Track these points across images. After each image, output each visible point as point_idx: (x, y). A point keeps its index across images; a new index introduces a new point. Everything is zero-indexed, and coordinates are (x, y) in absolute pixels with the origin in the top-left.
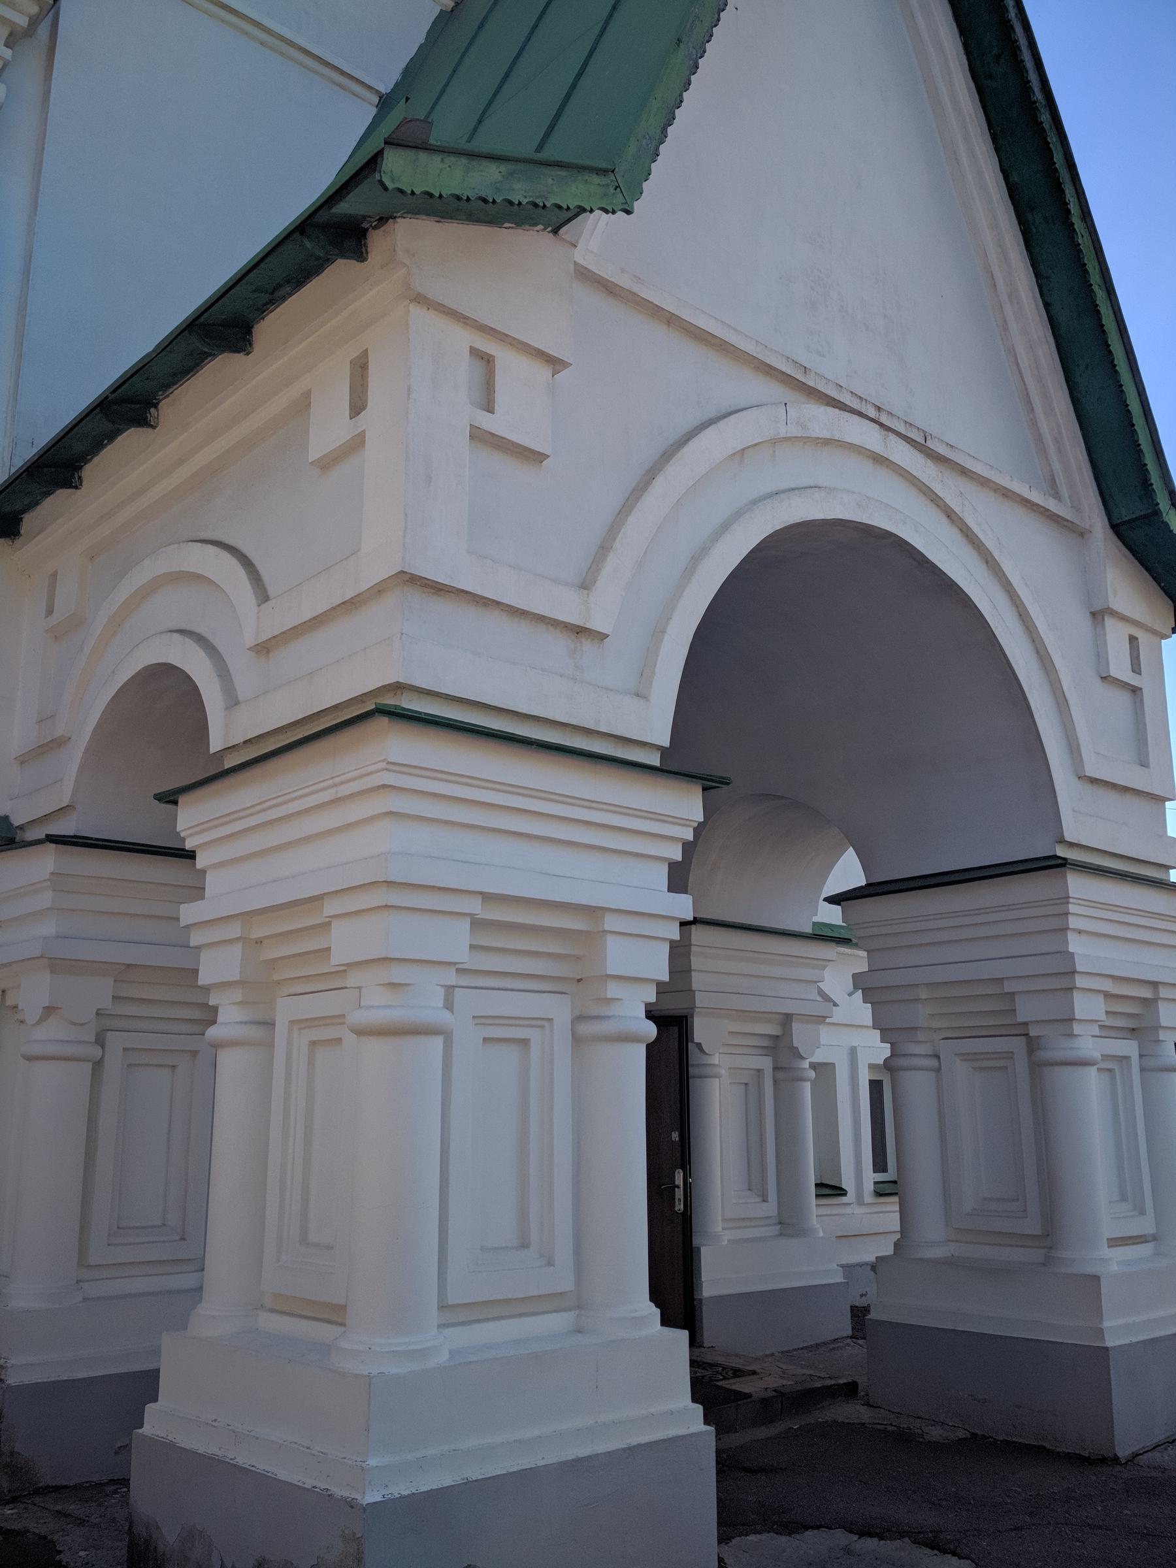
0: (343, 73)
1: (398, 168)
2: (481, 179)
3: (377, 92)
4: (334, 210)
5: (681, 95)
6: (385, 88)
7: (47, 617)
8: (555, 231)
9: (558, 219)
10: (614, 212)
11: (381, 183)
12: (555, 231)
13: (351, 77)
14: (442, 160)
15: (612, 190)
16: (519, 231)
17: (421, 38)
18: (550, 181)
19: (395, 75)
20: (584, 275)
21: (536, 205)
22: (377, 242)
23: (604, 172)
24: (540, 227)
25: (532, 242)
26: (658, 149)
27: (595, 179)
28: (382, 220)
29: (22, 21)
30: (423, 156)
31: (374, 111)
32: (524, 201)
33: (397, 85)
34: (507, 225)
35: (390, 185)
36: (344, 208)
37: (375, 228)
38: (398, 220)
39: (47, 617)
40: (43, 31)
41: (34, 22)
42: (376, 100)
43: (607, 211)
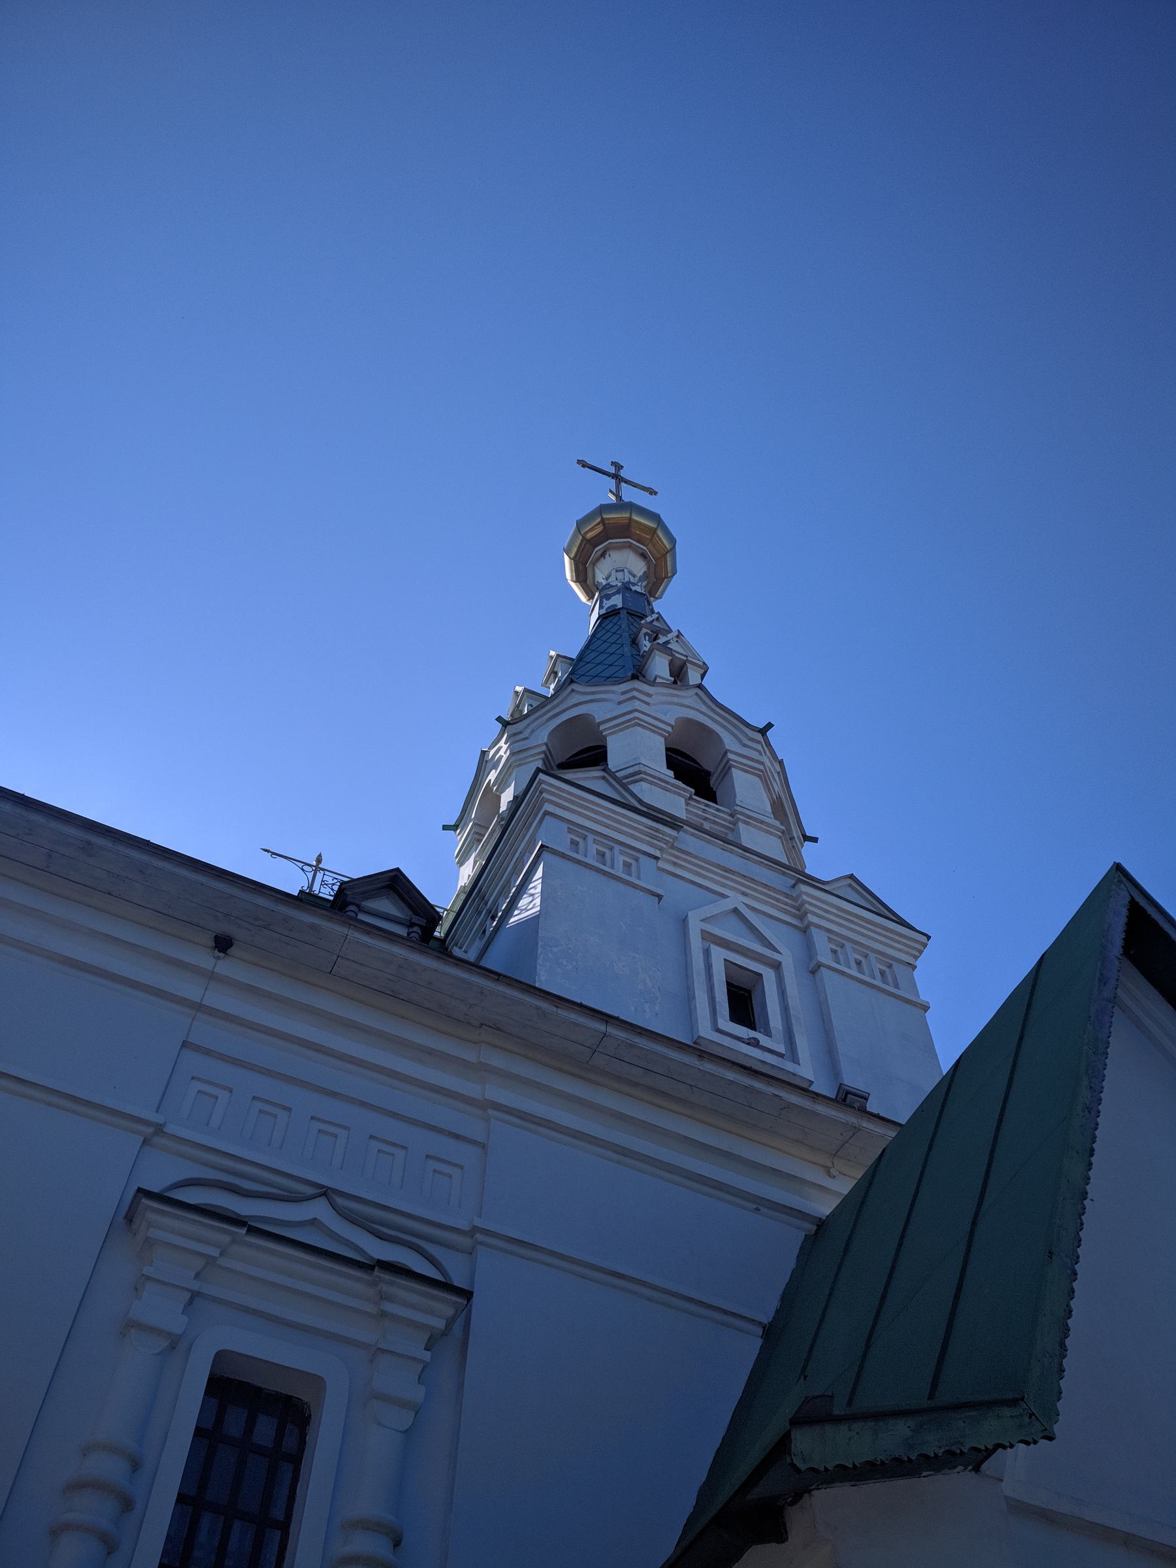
0: (725, 1312)
1: (808, 1446)
2: (893, 1438)
3: (760, 1323)
4: (749, 1497)
5: (1068, 1305)
6: (766, 1319)
7: (320, 855)
8: (977, 1469)
9: (977, 1459)
10: (1035, 1442)
11: (793, 1465)
12: (977, 1469)
13: (734, 1314)
14: (850, 1430)
15: (1027, 1420)
16: (939, 1477)
17: (792, 1264)
18: (961, 1424)
19: (773, 1304)
20: (1018, 1508)
21: (953, 1453)
22: (797, 1519)
23: (1013, 1403)
24: (960, 1468)
25: (957, 1481)
26: (1061, 1364)
27: (1007, 1412)
28: (797, 1497)
29: (440, 1324)
30: (829, 1428)
31: (760, 1342)
32: (940, 1452)
33: (777, 1311)
34: (925, 1474)
35: (802, 1467)
36: (759, 1492)
37: (792, 1504)
38: (814, 1493)
39: (320, 855)
40: (457, 1328)
41: (450, 1323)
42: (760, 1331)
43: (1028, 1443)
